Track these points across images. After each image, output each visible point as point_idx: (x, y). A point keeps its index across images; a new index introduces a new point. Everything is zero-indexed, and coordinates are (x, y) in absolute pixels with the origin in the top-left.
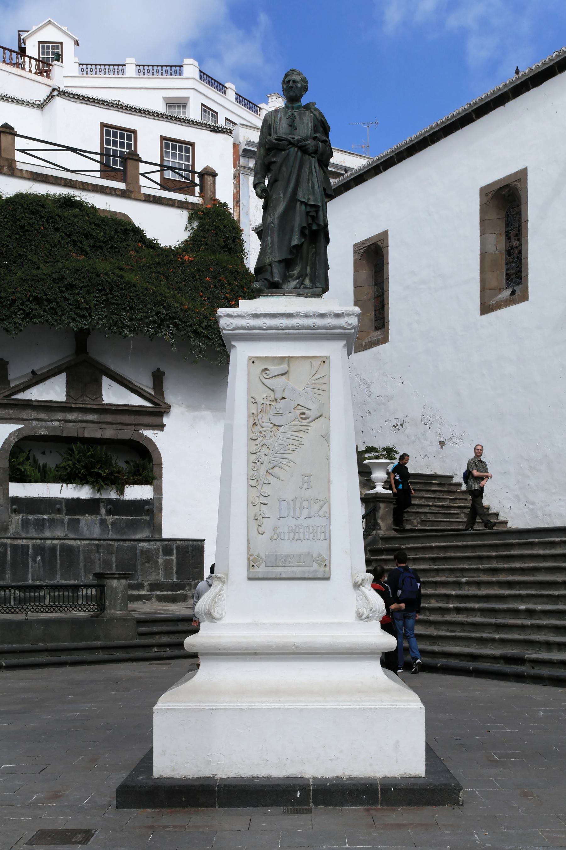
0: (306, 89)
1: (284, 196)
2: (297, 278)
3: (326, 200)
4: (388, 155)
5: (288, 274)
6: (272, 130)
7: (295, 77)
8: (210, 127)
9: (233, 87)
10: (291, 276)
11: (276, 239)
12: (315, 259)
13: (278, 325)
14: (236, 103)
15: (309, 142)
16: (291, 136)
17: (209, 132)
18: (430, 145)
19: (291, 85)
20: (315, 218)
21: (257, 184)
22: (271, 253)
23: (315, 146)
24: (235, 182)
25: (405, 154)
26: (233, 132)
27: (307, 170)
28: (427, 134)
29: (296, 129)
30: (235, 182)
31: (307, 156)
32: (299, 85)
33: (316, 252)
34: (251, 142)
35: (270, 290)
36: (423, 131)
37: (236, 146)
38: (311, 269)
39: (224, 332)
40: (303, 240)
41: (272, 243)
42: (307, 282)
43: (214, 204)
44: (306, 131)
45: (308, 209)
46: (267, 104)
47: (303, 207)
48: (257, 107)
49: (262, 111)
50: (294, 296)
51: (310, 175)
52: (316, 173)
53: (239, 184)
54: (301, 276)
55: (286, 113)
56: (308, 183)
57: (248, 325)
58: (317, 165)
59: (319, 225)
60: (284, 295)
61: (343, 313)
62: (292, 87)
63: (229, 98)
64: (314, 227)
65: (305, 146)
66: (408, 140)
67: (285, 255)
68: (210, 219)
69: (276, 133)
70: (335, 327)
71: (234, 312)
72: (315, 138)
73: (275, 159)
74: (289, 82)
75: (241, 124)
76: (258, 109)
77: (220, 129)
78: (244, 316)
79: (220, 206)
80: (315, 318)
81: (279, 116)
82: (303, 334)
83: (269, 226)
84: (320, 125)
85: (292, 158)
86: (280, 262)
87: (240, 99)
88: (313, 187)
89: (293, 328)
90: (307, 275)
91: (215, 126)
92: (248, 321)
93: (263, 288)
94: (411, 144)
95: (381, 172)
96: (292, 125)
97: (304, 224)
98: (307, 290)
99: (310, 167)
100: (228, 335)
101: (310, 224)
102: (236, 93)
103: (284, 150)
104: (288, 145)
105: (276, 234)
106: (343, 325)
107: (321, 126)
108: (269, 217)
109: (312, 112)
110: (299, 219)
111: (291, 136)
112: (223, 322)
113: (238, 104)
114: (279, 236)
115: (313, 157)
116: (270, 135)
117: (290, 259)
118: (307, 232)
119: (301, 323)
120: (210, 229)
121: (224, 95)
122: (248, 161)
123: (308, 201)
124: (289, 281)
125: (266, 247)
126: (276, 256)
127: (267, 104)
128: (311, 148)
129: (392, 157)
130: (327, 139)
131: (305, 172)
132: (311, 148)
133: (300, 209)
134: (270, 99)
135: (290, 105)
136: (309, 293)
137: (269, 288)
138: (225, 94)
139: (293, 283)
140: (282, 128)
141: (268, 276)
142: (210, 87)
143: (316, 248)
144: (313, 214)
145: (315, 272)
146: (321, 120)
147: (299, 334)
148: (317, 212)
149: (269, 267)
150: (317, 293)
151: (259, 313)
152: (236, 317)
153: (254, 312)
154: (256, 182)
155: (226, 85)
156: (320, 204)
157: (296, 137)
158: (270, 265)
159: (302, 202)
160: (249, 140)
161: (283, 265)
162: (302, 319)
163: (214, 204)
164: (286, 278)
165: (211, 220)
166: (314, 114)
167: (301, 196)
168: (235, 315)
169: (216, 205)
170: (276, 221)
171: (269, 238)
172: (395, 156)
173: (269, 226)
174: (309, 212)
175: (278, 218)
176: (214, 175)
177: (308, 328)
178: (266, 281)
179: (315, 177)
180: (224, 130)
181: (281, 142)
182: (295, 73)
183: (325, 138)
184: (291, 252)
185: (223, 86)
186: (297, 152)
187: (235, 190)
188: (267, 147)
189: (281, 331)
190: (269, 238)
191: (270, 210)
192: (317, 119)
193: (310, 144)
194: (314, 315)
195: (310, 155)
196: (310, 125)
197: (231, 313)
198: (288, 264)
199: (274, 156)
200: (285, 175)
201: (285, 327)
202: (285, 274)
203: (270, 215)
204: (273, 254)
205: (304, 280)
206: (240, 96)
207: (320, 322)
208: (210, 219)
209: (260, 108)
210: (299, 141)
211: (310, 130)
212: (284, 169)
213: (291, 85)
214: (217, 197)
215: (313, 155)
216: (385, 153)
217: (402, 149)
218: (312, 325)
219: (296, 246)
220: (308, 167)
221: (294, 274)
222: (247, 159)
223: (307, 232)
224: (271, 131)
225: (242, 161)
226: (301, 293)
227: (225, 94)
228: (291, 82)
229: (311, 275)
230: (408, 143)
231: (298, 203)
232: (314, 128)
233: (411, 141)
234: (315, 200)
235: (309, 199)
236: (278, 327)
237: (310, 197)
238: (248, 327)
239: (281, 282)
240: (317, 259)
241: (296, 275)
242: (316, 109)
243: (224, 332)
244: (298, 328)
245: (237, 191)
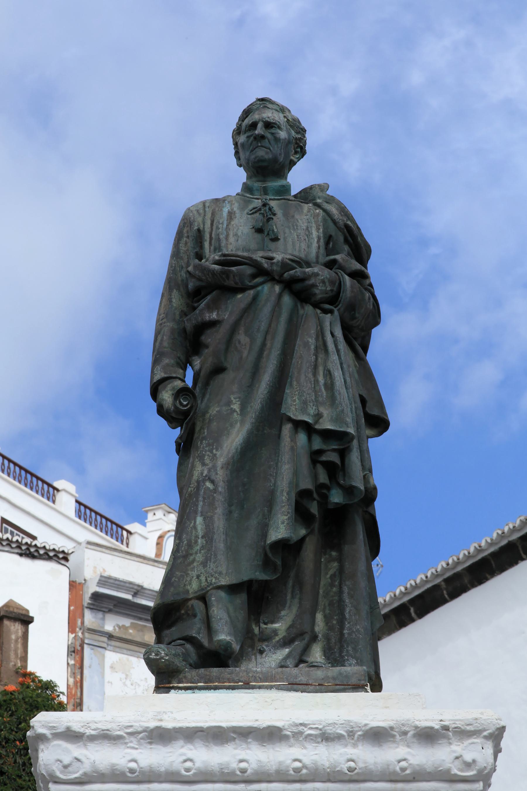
0: (300, 149)
1: (243, 407)
2: (287, 642)
4: (427, 582)
5: (256, 630)
6: (206, 245)
7: (269, 115)
8: (19, 547)
9: (71, 488)
10: (265, 638)
11: (219, 523)
13: (234, 765)
14: (77, 519)
15: (316, 270)
17: (17, 557)
19: (259, 130)
20: (336, 471)
22: (204, 564)
23: (332, 282)
24: (72, 662)
26: (71, 558)
27: (312, 341)
28: (515, 536)
29: (275, 239)
30: (72, 662)
31: (309, 309)
32: (283, 134)
33: (341, 570)
34: (109, 578)
35: (202, 671)
36: (506, 529)
37: (75, 587)
38: (327, 619)
40: (303, 532)
41: (208, 536)
42: (317, 654)
43: (22, 684)
44: (303, 246)
45: (318, 444)
46: (144, 525)
47: (302, 437)
48: (123, 528)
50: (279, 688)
51: (321, 356)
52: (338, 351)
53: (81, 668)
54: (300, 639)
55: (247, 202)
56: (315, 374)
57: (133, 765)
58: (339, 332)
59: (349, 490)
61: (446, 728)
62: (263, 137)
63: (62, 510)
64: (336, 497)
65: (302, 280)
66: (472, 550)
67: (249, 571)
68: (11, 715)
69: (218, 248)
71: (87, 725)
72: (331, 265)
73: (214, 316)
74: (254, 125)
75: (89, 543)
76: (125, 533)
77: (42, 552)
79: (38, 688)
80: (355, 745)
81: (226, 210)
83: (198, 488)
84: (341, 239)
85: (266, 311)
86: (232, 589)
87: (84, 511)
88: (330, 386)
90: (314, 638)
92: (135, 754)
93: (178, 662)
95: (413, 620)
96: (263, 230)
97: (307, 484)
98: (319, 674)
102: (77, 501)
103: (243, 290)
104: (254, 276)
105: (219, 511)
106: (447, 765)
110: (289, 468)
111: (261, 254)
114: (229, 514)
116: (200, 256)
117: (265, 585)
118: (314, 509)
119: (307, 761)
120: (12, 737)
121: (50, 503)
122: (103, 619)
123: (317, 422)
124: (261, 652)
125: (190, 545)
128: (321, 287)
129: (436, 587)
130: (363, 268)
131: (306, 345)
132: (321, 287)
133: (293, 447)
134: (150, 516)
135: (257, 185)
136: (326, 679)
137: (196, 666)
138: (54, 502)
139: (273, 658)
140: (238, 236)
141: (195, 629)
142: (23, 487)
143: (340, 560)
144: (334, 457)
145: (342, 628)
146: (347, 226)
148: (343, 453)
149: (199, 606)
151: (169, 724)
152: (92, 738)
153: (152, 724)
154: (157, 377)
155: (56, 484)
156: (351, 430)
157: (278, 257)
158: (203, 598)
159: (298, 425)
160: (106, 574)
161: (242, 599)
162: (310, 746)
163: (22, 684)
164: (252, 642)
165: (14, 718)
166: (325, 210)
167: (293, 407)
168: (89, 732)
169: (28, 687)
170: (221, 475)
171: (199, 520)
172: (443, 585)
173: (198, 488)
174: (320, 452)
175: (225, 466)
176: (26, 620)
178: (188, 646)
181: (233, 269)
182: (270, 106)
183: (357, 266)
184: (267, 564)
185: (50, 485)
186: (280, 296)
187: (71, 680)
190: (199, 520)
191: (202, 445)
192: (334, 222)
193: (317, 275)
194: (351, 734)
195: (316, 305)
196: (315, 234)
197: (76, 727)
198: (256, 598)
199: (213, 306)
200: (245, 353)
201: (256, 773)
202: (249, 631)
203: (201, 459)
204: (211, 565)
205: (306, 649)
206: (86, 507)
208: (11, 715)
209: (129, 532)
210: (285, 266)
211: (315, 245)
212: (242, 337)
213: (259, 130)
214: (31, 668)
215: (327, 306)
216: (420, 578)
217: (459, 568)
218: (344, 767)
220: (313, 331)
221: (275, 632)
222: (100, 615)
223: (314, 509)
224: (202, 247)
225: (90, 618)
226: (303, 679)
227: (54, 502)
228: (260, 125)
229: (327, 638)
230: (473, 557)
231: (287, 428)
232: (327, 244)
233: (479, 550)
234: (339, 419)
235: (319, 416)
236: (233, 773)
238: (132, 771)
239: (236, 647)
240: (346, 589)
241: (282, 634)
242: (331, 200)
245: (75, 683)
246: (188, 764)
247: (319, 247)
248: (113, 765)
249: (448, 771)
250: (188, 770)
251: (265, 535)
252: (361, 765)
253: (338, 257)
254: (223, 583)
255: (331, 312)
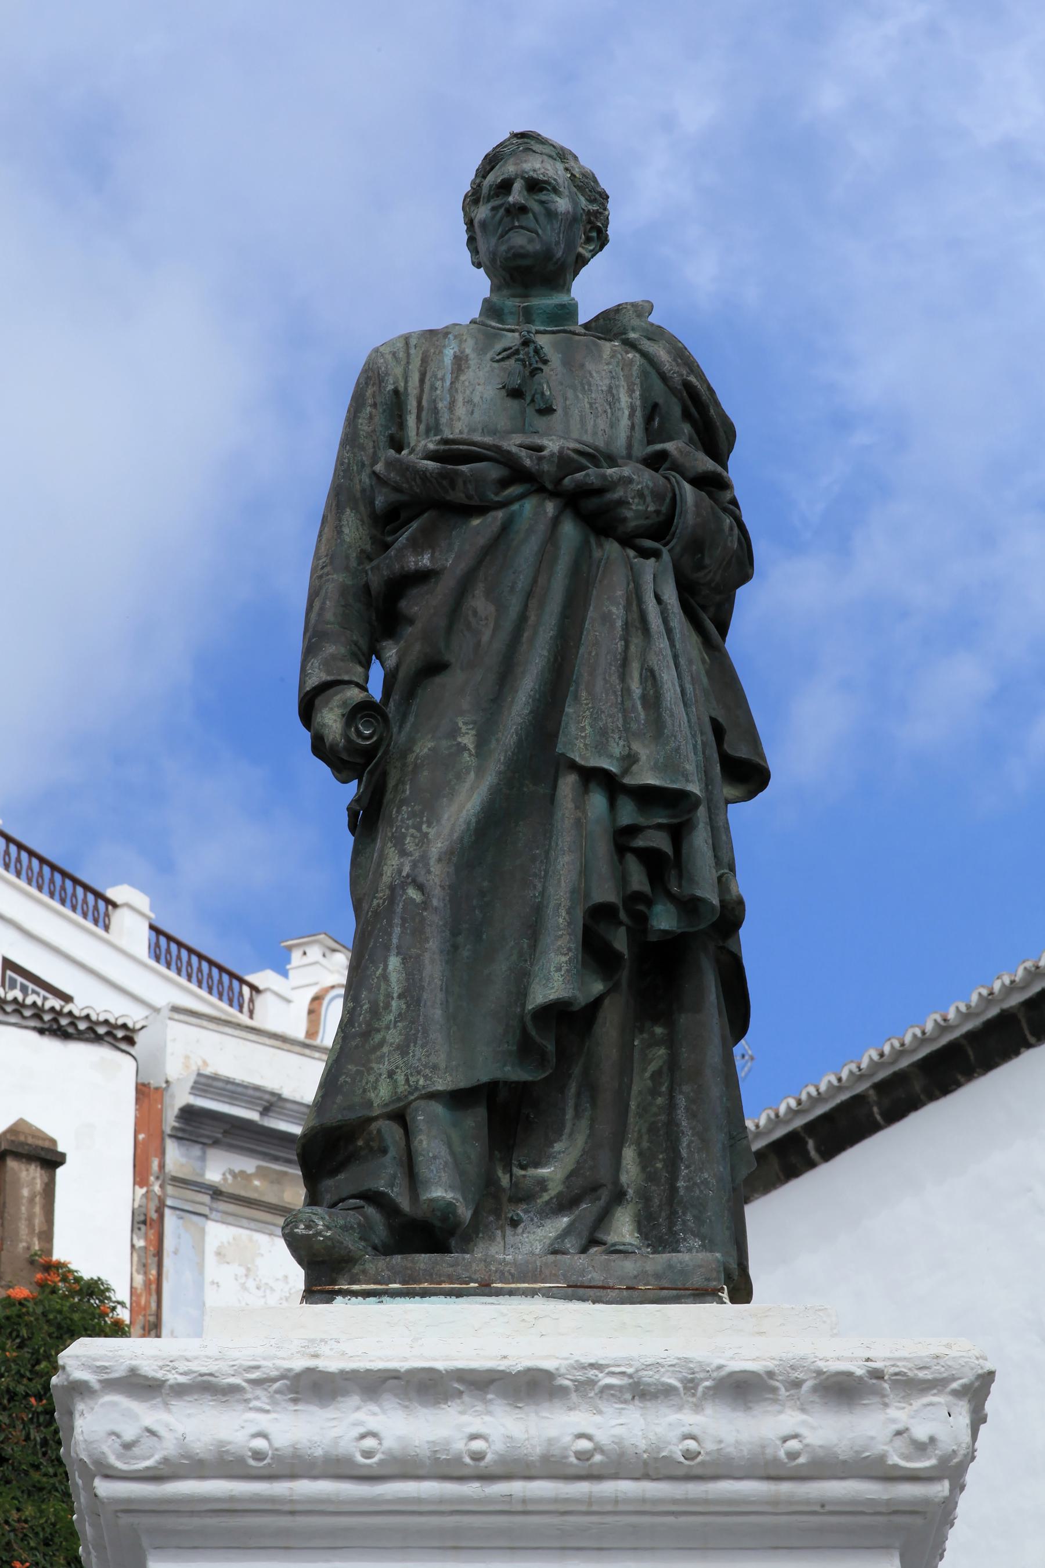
1: (482, 742)
2: (564, 1204)
3: (729, 791)
4: (840, 1089)
5: (505, 1181)
6: (411, 421)
7: (536, 165)
8: (38, 1016)
9: (142, 901)
10: (523, 1196)
11: (433, 970)
12: (671, 1106)
13: (459, 1445)
14: (153, 963)
16: (518, 439)
17: (34, 1036)
18: (1029, 1046)
19: (517, 195)
20: (664, 867)
21: (324, 687)
22: (403, 1050)
23: (658, 496)
24: (140, 1243)
25: (917, 1086)
26: (139, 1038)
27: (617, 612)
28: (1016, 1000)
29: (547, 411)
30: (140, 1243)
31: (612, 548)
32: (562, 204)
33: (673, 1064)
34: (215, 1078)
35: (397, 1259)
36: (997, 986)
38: (645, 1159)
39: (104, 1488)
40: (598, 987)
41: (412, 994)
42: (623, 1228)
43: (42, 1285)
44: (602, 424)
45: (628, 814)
46: (285, 974)
47: (597, 801)
48: (242, 981)
49: (259, 1001)
50: (549, 1294)
51: (636, 641)
52: (669, 631)
53: (159, 1254)
54: (590, 1200)
56: (623, 677)
57: (260, 1444)
59: (690, 906)
60: (486, 1289)
61: (877, 1375)
62: (523, 209)
64: (664, 919)
65: (600, 491)
66: (929, 1026)
67: (489, 1064)
68: (20, 1346)
69: (433, 428)
70: (825, 1466)
72: (656, 461)
73: (425, 561)
74: (505, 186)
75: (175, 1009)
76: (246, 990)
77: (82, 1026)
78: (233, 1390)
79: (73, 1293)
80: (698, 1408)
81: (449, 353)
82: (616, 1507)
83: (392, 899)
84: (677, 411)
86: (459, 1099)
87: (166, 946)
88: (653, 701)
89: (551, 1466)
90: (619, 1196)
91: (60, 1013)
92: (263, 1421)
93: (351, 1243)
94: (944, 1041)
95: (812, 1165)
97: (605, 893)
98: (629, 1266)
99: (635, 597)
100: (129, 1507)
101: (637, 897)
102: (152, 927)
103: (483, 510)
104: (504, 483)
106: (880, 1448)
107: (687, 415)
108: (392, 852)
109: (632, 345)
110: (572, 861)
111: (518, 439)
112: (95, 1427)
113: (162, 968)
114: (452, 952)
115: (645, 554)
116: (397, 444)
118: (620, 941)
119: (603, 1437)
120: (21, 1389)
121: (100, 931)
122: (203, 1159)
123: (626, 771)
124: (515, 1223)
125: (375, 1012)
126: (439, 1061)
127: (285, 974)
128: (636, 505)
129: (858, 1100)
130: (719, 469)
131: (606, 618)
132: (636, 505)
133: (579, 821)
134: (296, 956)
135: (512, 304)
137: (385, 1250)
138: (107, 928)
140: (472, 404)
141: (385, 1178)
143: (671, 1042)
144: (660, 841)
145: (674, 1177)
146: (687, 386)
147: (590, 1507)
148: (678, 833)
149: (392, 1132)
150: (697, 1281)
151: (331, 1364)
152: (180, 1391)
153: (299, 1364)
154: (312, 682)
155: (111, 893)
156: (695, 788)
157: (552, 445)
158: (400, 1117)
159: (591, 776)
160: (208, 1071)
161: (476, 1119)
162: (610, 1409)
163: (42, 1285)
164: (500, 1201)
165: (26, 1353)
166: (644, 355)
167: (580, 742)
168: (174, 1378)
170: (437, 875)
171: (394, 962)
173: (392, 899)
174: (632, 830)
176: (50, 1160)
177: (652, 1467)
178: (370, 1210)
179: (662, 643)
180: (101, 1030)
181: (464, 468)
182: (537, 147)
184: (526, 1049)
185: (99, 895)
186: (556, 522)
187: (139, 1279)
188: (380, 501)
189: (472, 1489)
190: (394, 962)
192: (663, 377)
193: (630, 481)
194: (690, 1384)
195: (626, 541)
196: (624, 400)
197: (149, 1369)
198: (506, 1117)
199: (423, 542)
202: (490, 1183)
204: (417, 1052)
205: (603, 1218)
206: (170, 938)
207: (726, 1429)
208: (20, 1346)
209: (254, 988)
210: (566, 463)
211: (625, 422)
212: (479, 603)
213: (517, 195)
214: (59, 1254)
215: (648, 543)
217: (904, 1063)
218: (676, 1450)
219: (557, 1014)
221: (542, 1184)
222: (196, 1151)
223: (620, 941)
224: (402, 425)
225: (176, 1157)
227: (107, 928)
228: (518, 186)
231: (568, 783)
232: (649, 420)
233: (943, 1027)
234: (670, 765)
235: (630, 760)
236: (458, 1460)
237: (636, 746)
238: (258, 1455)
239: (465, 1213)
240: (681, 1101)
241: (555, 1188)
242: (656, 334)
243: (104, 1488)
244: (588, 1468)
245: (147, 1283)
246: (369, 1443)
247: (633, 427)
248: (221, 1444)
249: (882, 1458)
250: (368, 1454)
251: (522, 994)
252: (710, 1446)
253: (670, 446)
254: (440, 1087)
255: (656, 554)
